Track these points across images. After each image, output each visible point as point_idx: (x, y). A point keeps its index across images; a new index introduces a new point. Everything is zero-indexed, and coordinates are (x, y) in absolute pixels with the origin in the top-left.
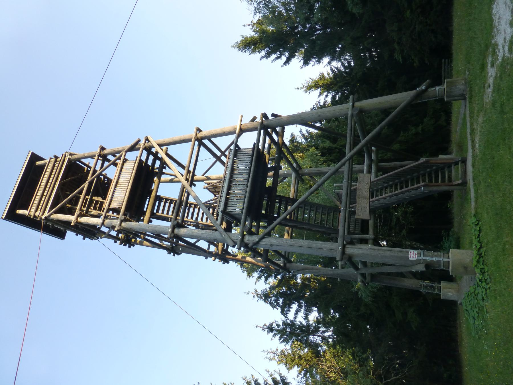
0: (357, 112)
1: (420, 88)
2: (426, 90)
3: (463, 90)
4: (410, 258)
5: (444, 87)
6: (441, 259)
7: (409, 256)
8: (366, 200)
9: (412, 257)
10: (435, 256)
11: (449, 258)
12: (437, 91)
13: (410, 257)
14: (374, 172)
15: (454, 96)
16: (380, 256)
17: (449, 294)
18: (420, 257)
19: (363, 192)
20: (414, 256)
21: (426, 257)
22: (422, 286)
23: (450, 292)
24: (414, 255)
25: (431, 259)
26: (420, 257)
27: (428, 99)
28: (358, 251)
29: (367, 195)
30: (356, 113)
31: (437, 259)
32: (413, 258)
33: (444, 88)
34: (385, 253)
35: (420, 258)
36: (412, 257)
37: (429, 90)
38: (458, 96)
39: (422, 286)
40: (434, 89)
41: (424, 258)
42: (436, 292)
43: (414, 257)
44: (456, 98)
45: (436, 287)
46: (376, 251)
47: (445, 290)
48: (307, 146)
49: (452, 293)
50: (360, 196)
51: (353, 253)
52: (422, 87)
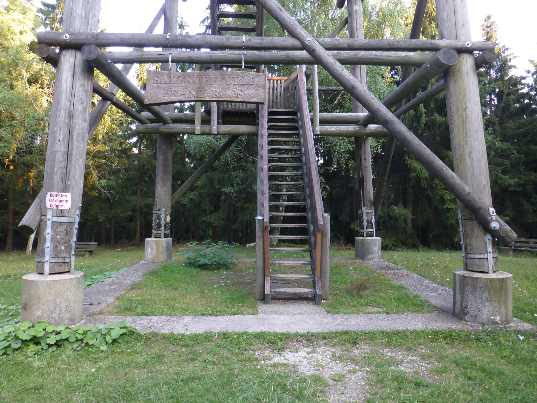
0: (440, 59)
1: (494, 216)
2: (486, 228)
3: (476, 317)
4: (49, 194)
5: (491, 271)
6: (47, 258)
7: (53, 193)
8: (194, 93)
9: (52, 198)
10: (57, 247)
11: (50, 274)
12: (482, 256)
13: (51, 195)
14: (341, 129)
15: (462, 293)
16: (55, 129)
17: (150, 250)
18: (53, 216)
19: (216, 85)
20: (54, 203)
21: (52, 227)
22: (159, 212)
23: (152, 250)
24: (57, 204)
25: (48, 237)
26: (53, 216)
27: (463, 234)
28: (66, 81)
29: (206, 95)
30: (438, 58)
31: (47, 250)
32: (50, 201)
33: (487, 273)
34: (61, 141)
35: (49, 216)
36: (52, 198)
37: (488, 237)
38: (462, 302)
39: (159, 212)
40: (490, 249)
41: (49, 223)
42: (154, 232)
43: (51, 203)
44: (459, 297)
45: (159, 232)
46: (67, 121)
47: (154, 245)
48: (433, 34)
49: (151, 253)
50: (204, 79)
51: (62, 70)
52: (497, 221)
